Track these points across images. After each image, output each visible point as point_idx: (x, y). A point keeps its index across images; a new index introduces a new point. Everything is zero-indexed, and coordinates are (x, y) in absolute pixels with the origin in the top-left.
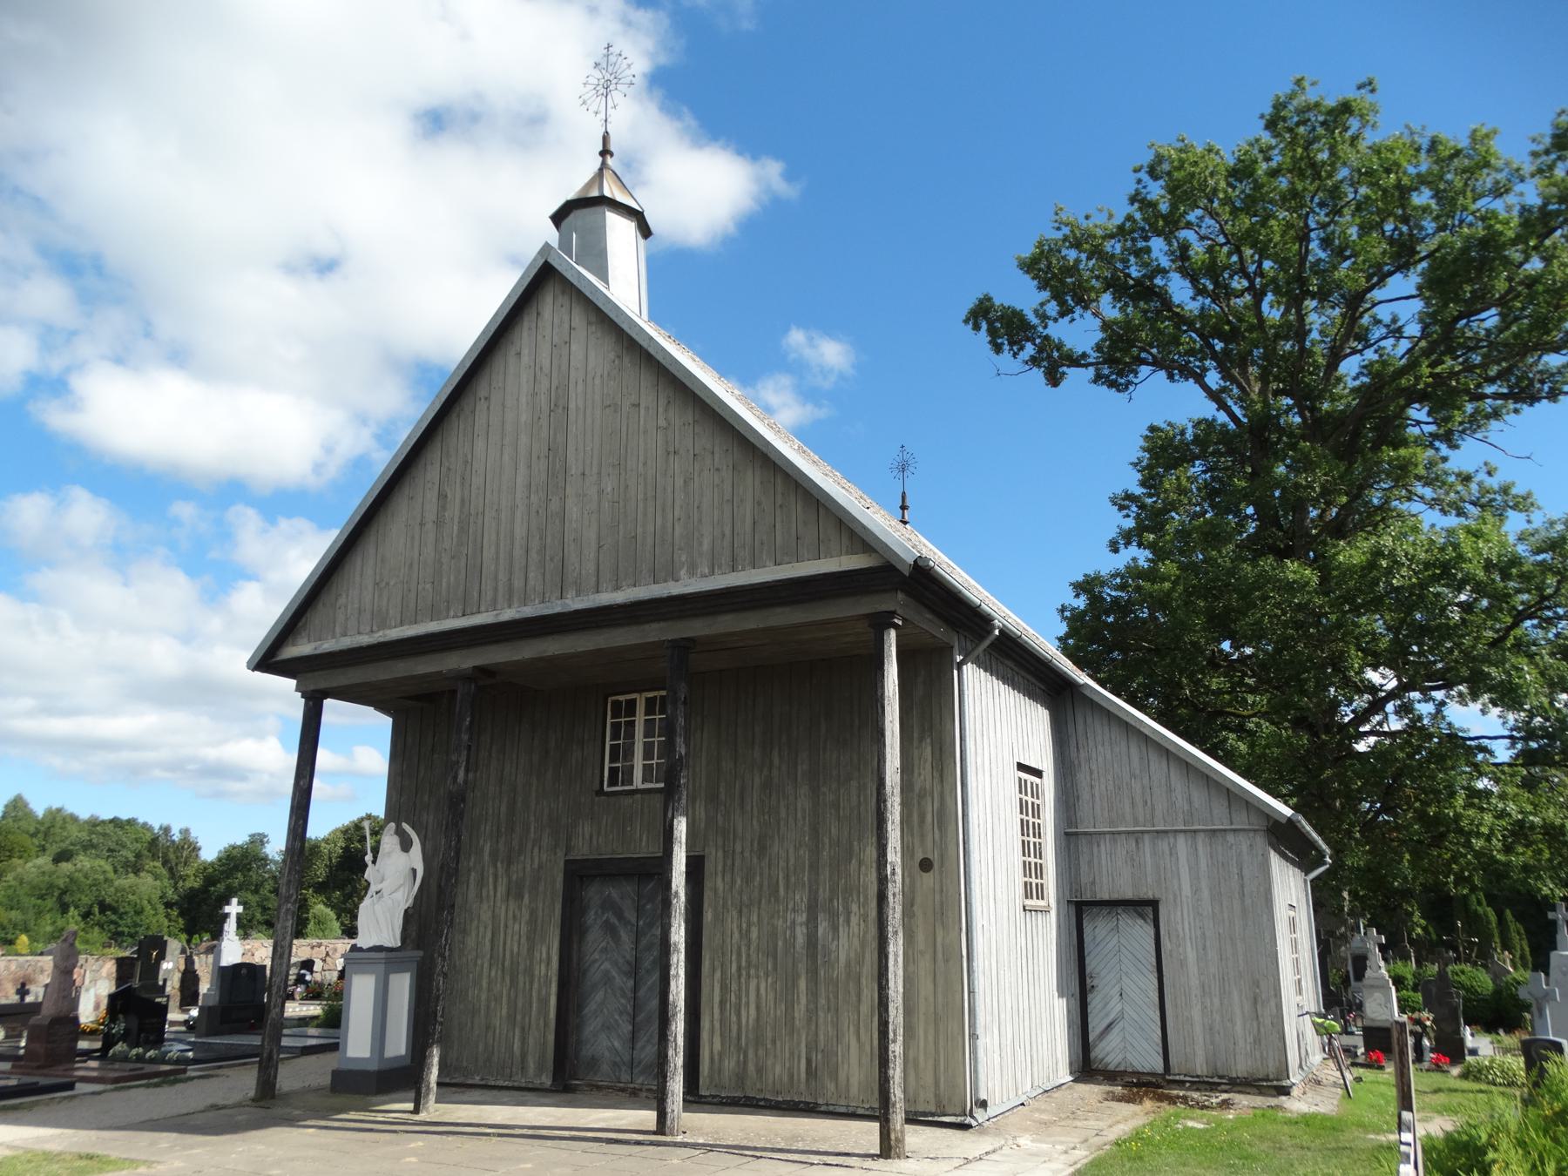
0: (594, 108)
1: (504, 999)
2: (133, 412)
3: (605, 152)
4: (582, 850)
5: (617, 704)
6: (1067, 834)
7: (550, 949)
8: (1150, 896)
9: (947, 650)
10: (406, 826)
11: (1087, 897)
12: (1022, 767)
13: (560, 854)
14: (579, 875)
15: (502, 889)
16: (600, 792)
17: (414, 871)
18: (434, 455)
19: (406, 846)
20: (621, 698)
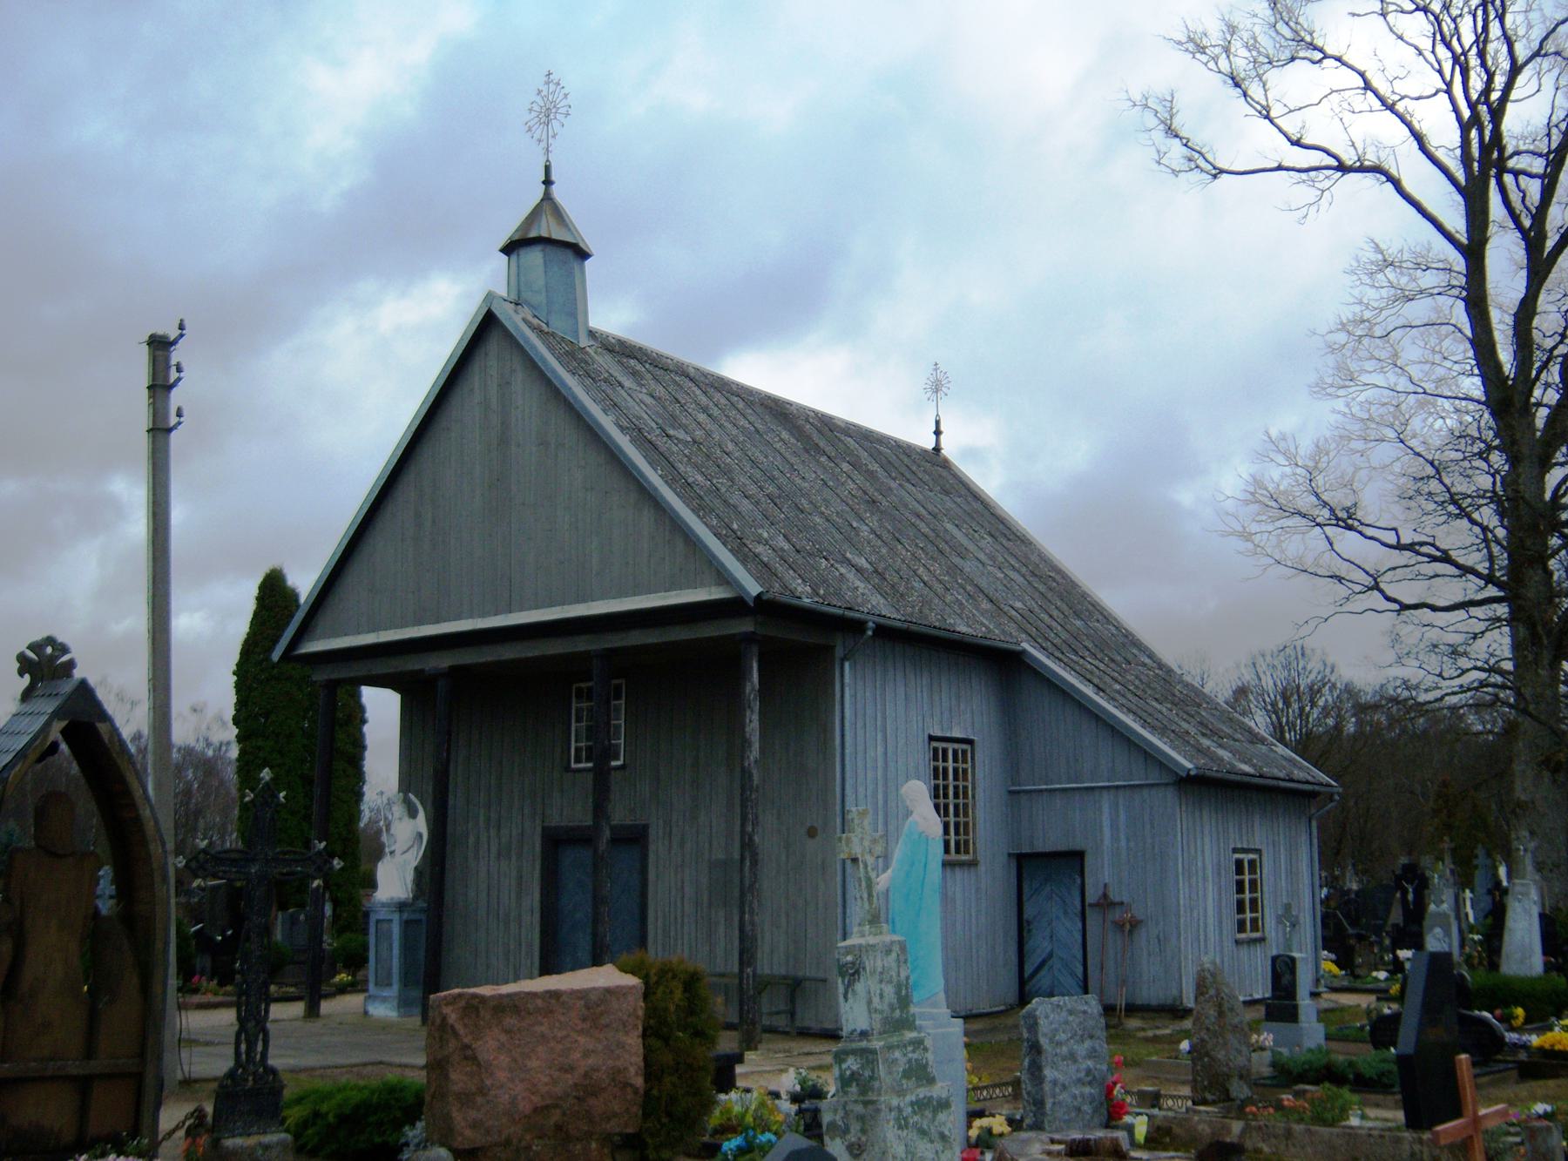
0: (536, 136)
1: (172, 881)
2: (285, 1013)
3: (548, 182)
4: (556, 819)
5: (579, 691)
6: (1010, 792)
7: (534, 897)
8: (1078, 848)
9: (829, 649)
10: (412, 796)
11: (1026, 850)
12: (932, 738)
13: (538, 822)
14: (556, 842)
15: (494, 850)
16: (568, 769)
17: (420, 835)
18: (409, 477)
19: (413, 814)
20: (583, 685)
